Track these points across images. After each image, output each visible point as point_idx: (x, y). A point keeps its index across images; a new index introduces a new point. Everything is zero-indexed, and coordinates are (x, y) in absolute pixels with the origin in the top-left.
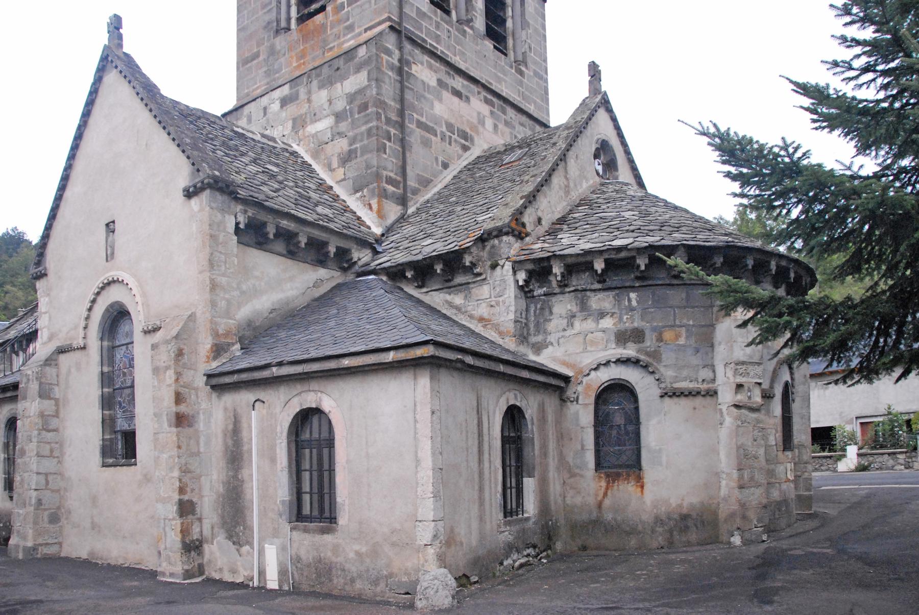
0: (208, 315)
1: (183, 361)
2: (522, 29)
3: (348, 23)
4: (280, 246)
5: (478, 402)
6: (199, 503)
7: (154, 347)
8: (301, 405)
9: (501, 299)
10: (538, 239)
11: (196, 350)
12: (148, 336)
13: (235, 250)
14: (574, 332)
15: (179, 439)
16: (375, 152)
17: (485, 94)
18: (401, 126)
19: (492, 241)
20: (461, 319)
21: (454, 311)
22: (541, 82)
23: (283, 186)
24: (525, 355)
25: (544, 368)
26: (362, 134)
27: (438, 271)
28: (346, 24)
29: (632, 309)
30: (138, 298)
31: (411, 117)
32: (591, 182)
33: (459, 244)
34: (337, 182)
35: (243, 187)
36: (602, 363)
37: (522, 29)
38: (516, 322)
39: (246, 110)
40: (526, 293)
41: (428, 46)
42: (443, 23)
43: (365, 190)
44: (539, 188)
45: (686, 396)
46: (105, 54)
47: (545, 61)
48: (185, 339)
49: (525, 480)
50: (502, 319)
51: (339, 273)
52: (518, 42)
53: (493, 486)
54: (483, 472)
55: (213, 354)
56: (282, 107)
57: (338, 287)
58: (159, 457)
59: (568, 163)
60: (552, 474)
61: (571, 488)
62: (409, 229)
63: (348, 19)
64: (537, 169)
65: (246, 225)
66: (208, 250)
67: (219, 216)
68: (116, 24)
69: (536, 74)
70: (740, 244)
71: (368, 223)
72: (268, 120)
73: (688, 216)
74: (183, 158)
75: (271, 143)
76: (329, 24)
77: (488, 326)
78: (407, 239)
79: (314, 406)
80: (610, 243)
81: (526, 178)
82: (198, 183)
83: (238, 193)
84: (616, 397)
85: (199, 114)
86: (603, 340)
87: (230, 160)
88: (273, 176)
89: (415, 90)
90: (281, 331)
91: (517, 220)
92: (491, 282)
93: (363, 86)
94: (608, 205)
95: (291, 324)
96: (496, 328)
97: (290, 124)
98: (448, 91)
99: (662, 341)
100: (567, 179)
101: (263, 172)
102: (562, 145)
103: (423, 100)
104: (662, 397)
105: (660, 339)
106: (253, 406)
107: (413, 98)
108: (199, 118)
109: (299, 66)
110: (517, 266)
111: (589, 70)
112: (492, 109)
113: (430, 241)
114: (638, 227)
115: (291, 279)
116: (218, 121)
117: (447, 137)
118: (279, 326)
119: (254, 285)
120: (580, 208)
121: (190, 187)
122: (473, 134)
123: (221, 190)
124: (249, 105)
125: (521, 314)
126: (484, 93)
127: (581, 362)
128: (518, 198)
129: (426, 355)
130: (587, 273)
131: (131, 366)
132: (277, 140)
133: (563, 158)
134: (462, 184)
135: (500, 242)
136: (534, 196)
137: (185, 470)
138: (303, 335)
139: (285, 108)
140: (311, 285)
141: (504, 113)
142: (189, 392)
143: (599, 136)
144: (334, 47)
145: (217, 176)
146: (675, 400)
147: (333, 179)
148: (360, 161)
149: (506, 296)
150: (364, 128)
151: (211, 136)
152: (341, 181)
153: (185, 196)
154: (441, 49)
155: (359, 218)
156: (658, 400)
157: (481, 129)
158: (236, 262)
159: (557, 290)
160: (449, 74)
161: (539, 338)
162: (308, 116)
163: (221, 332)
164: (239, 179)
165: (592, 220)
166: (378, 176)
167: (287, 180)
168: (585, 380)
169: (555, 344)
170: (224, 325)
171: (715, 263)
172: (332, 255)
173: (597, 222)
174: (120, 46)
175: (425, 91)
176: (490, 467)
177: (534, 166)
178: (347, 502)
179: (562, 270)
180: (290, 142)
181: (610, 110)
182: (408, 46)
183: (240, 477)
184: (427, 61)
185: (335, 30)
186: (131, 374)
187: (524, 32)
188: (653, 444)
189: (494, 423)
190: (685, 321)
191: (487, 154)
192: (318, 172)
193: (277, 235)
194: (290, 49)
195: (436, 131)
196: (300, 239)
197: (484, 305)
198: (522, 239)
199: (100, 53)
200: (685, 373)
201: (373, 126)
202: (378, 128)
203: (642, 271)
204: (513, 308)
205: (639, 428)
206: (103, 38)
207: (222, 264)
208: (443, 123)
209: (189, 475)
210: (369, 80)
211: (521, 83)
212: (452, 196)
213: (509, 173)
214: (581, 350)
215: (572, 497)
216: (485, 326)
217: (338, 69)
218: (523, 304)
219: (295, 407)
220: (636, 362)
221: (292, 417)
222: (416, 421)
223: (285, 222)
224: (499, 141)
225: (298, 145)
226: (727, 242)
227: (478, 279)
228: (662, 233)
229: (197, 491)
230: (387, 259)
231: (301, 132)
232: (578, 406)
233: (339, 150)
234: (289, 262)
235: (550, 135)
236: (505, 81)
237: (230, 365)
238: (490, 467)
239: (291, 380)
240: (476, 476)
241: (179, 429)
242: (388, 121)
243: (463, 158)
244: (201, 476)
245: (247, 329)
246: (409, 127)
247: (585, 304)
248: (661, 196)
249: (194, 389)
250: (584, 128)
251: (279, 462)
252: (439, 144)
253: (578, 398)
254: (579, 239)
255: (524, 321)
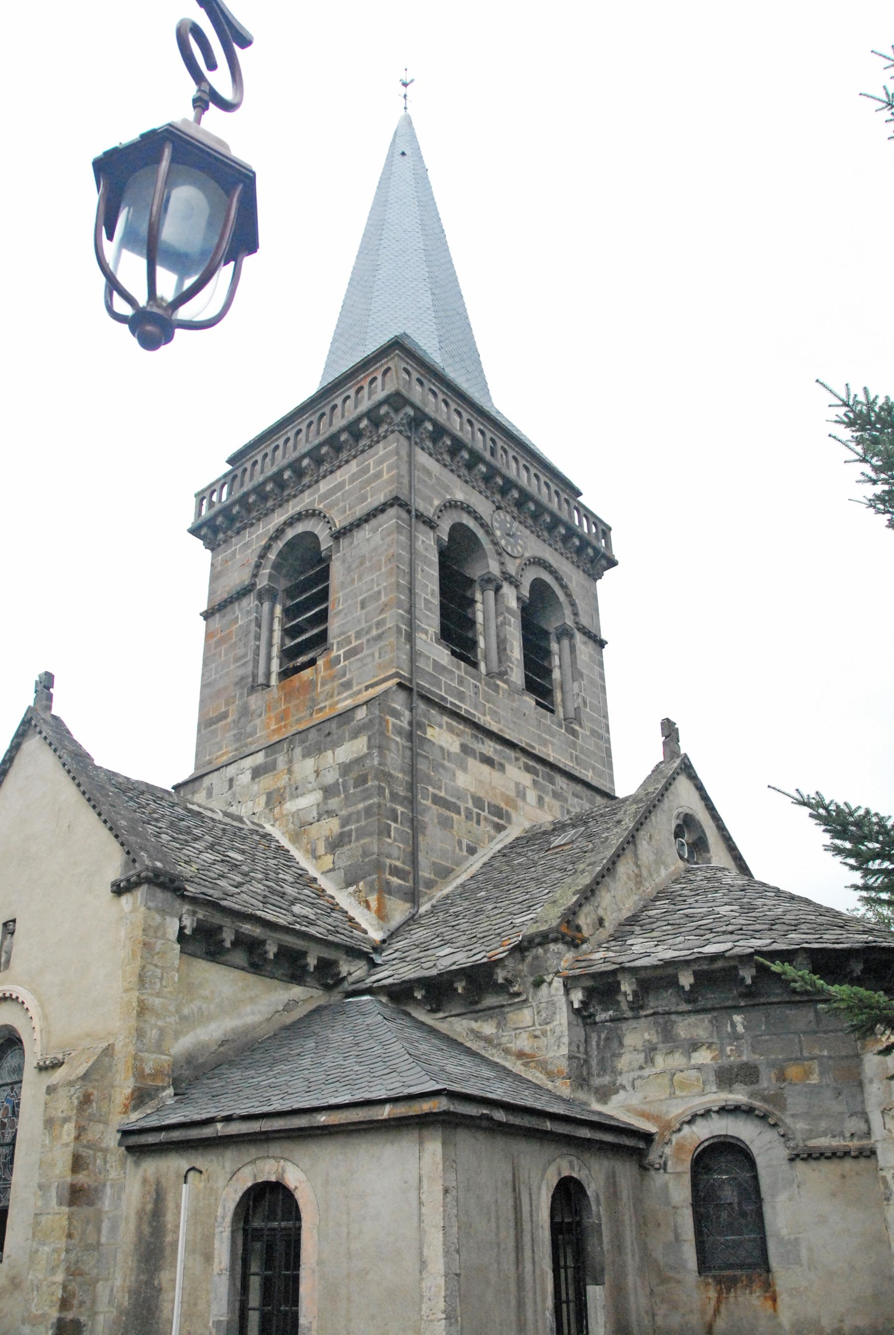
0: (131, 1049)
1: (90, 1111)
2: (573, 681)
3: (345, 679)
4: (240, 957)
5: (514, 1175)
6: (90, 1323)
7: (50, 1090)
8: (255, 1176)
9: (548, 1027)
10: (600, 946)
11: (110, 1096)
12: (44, 1074)
13: (177, 962)
14: (654, 1070)
15: (70, 1224)
16: (376, 836)
17: (526, 760)
18: (411, 802)
19: (534, 951)
20: (493, 1055)
21: (483, 1044)
22: (601, 743)
23: (248, 879)
24: (585, 1104)
25: (613, 1123)
26: (358, 812)
27: (460, 991)
28: (340, 681)
29: (737, 1037)
30: (36, 1023)
31: (425, 791)
32: (673, 868)
33: (488, 954)
34: (323, 873)
35: (192, 882)
36: (699, 1113)
37: (573, 681)
38: (571, 1058)
39: (206, 781)
40: (584, 1018)
41: (449, 706)
42: (468, 678)
43: (361, 884)
44: (599, 879)
45: (828, 1158)
46: (29, 716)
47: (606, 717)
48: (96, 1080)
49: (590, 1288)
50: (551, 1054)
51: (320, 992)
52: (569, 696)
53: (539, 1299)
54: (523, 1279)
55: (133, 1103)
56: (253, 778)
57: (318, 1010)
58: (37, 1251)
59: (639, 846)
60: (632, 1280)
61: (662, 1301)
62: (421, 934)
63: (344, 675)
64: (595, 855)
65: (194, 931)
66: (138, 962)
67: (158, 918)
68: (46, 683)
69: (594, 732)
70: (885, 944)
71: (364, 925)
72: (234, 795)
73: (811, 908)
74: (115, 845)
75: (235, 824)
76: (319, 681)
77: (532, 1064)
78: (418, 946)
79: (273, 1179)
80: (700, 950)
81: (582, 866)
82: (132, 876)
83: (186, 890)
84: (723, 1161)
85: (143, 788)
86: (698, 1080)
87: (178, 846)
88: (235, 867)
89: (431, 757)
90: (234, 1070)
91: (568, 922)
92: (534, 1004)
93: (362, 754)
94: (697, 898)
95: (250, 1061)
96: (543, 1066)
97: (263, 800)
98: (475, 758)
99: (784, 1080)
100: (638, 866)
101: (222, 861)
102: (629, 823)
103: (441, 770)
104: (792, 1160)
105: (782, 1077)
106: (186, 1177)
107: (429, 768)
108: (142, 793)
109: (278, 730)
110: (569, 984)
111: (662, 729)
112: (536, 778)
113: (448, 950)
114: (739, 927)
115: (252, 1000)
116: (166, 796)
117: (475, 816)
118: (231, 1064)
119: (200, 1008)
120: (658, 903)
121: (121, 881)
122: (509, 809)
123: (163, 886)
124: (210, 776)
125: (578, 1047)
126: (524, 759)
127: (668, 1112)
128: (570, 893)
129: (436, 1110)
130: (670, 991)
131: (15, 1114)
132: (245, 819)
133: (631, 839)
134: (496, 875)
135: (546, 952)
136: (592, 891)
137: (74, 1272)
138: (264, 1077)
139: (257, 780)
140: (281, 1008)
141: (552, 782)
142: (94, 1154)
143: (680, 810)
144: (325, 707)
145: (158, 868)
146: (813, 1164)
147: (317, 869)
148: (354, 846)
149: (555, 1023)
150: (361, 806)
151: (155, 816)
152: (328, 871)
153: (113, 892)
154: (465, 708)
155: (351, 919)
156: (786, 1166)
157: (520, 803)
158: (176, 979)
159: (629, 1014)
160: (476, 737)
161: (606, 1079)
162: (288, 789)
163: (147, 1071)
164: (188, 871)
165: (675, 918)
166: (378, 867)
167: (253, 870)
168: (675, 1138)
169: (629, 1088)
170: (150, 1064)
171: (852, 972)
172: (312, 969)
173: (682, 921)
174: (49, 708)
175: (444, 759)
176: (534, 1272)
177: (592, 851)
178: (315, 1325)
179: (634, 987)
180: (262, 822)
181: (693, 777)
182: (422, 706)
183: (156, 1282)
184: (447, 723)
185: (327, 687)
186: (14, 1125)
187: (576, 685)
188: (784, 1232)
189: (539, 1204)
190: (816, 1052)
191: (530, 834)
192: (297, 860)
193: (235, 944)
194: (269, 708)
195: (459, 808)
196: (268, 947)
197: (525, 1035)
198: (576, 946)
199: (22, 716)
200: (823, 1125)
201: (374, 804)
202: (379, 806)
203: (747, 986)
204: (566, 1040)
205: (761, 1207)
206: (28, 699)
207: (157, 980)
208: (469, 797)
209: (79, 1279)
210: (370, 747)
211: (574, 745)
212: (481, 889)
213: (559, 859)
214: (667, 1096)
215: (665, 1316)
216: (526, 1065)
217: (329, 734)
218: (581, 1032)
219: (246, 1180)
220: (748, 1111)
221: (240, 1194)
222: (421, 1203)
223: (248, 926)
224: (546, 818)
225: (273, 825)
226: (866, 943)
227: (516, 1000)
228: (774, 934)
229: (88, 1304)
230: (385, 975)
231: (277, 810)
232: (667, 1176)
233: (328, 833)
234: (251, 978)
235: (614, 810)
236: (553, 744)
237: (157, 1117)
238: (534, 1272)
239: (243, 1142)
240: (513, 1287)
241: (74, 1208)
242: (394, 796)
243: (495, 841)
244: (98, 1281)
245: (185, 1067)
246: (421, 804)
247: (670, 1031)
248: (772, 883)
249: (101, 1150)
250: (659, 801)
251: (216, 1261)
252: (463, 824)
253: (665, 1164)
254: (656, 945)
255: (582, 1056)
